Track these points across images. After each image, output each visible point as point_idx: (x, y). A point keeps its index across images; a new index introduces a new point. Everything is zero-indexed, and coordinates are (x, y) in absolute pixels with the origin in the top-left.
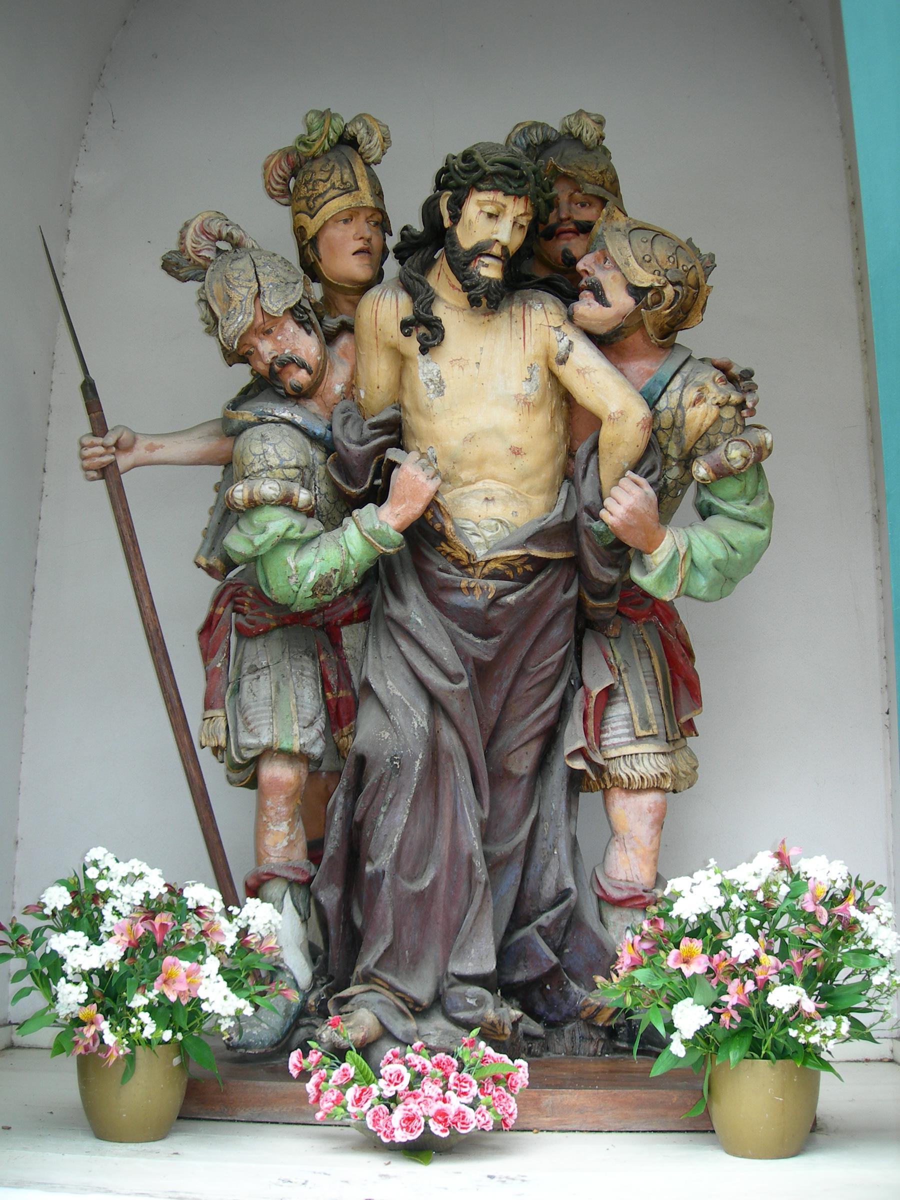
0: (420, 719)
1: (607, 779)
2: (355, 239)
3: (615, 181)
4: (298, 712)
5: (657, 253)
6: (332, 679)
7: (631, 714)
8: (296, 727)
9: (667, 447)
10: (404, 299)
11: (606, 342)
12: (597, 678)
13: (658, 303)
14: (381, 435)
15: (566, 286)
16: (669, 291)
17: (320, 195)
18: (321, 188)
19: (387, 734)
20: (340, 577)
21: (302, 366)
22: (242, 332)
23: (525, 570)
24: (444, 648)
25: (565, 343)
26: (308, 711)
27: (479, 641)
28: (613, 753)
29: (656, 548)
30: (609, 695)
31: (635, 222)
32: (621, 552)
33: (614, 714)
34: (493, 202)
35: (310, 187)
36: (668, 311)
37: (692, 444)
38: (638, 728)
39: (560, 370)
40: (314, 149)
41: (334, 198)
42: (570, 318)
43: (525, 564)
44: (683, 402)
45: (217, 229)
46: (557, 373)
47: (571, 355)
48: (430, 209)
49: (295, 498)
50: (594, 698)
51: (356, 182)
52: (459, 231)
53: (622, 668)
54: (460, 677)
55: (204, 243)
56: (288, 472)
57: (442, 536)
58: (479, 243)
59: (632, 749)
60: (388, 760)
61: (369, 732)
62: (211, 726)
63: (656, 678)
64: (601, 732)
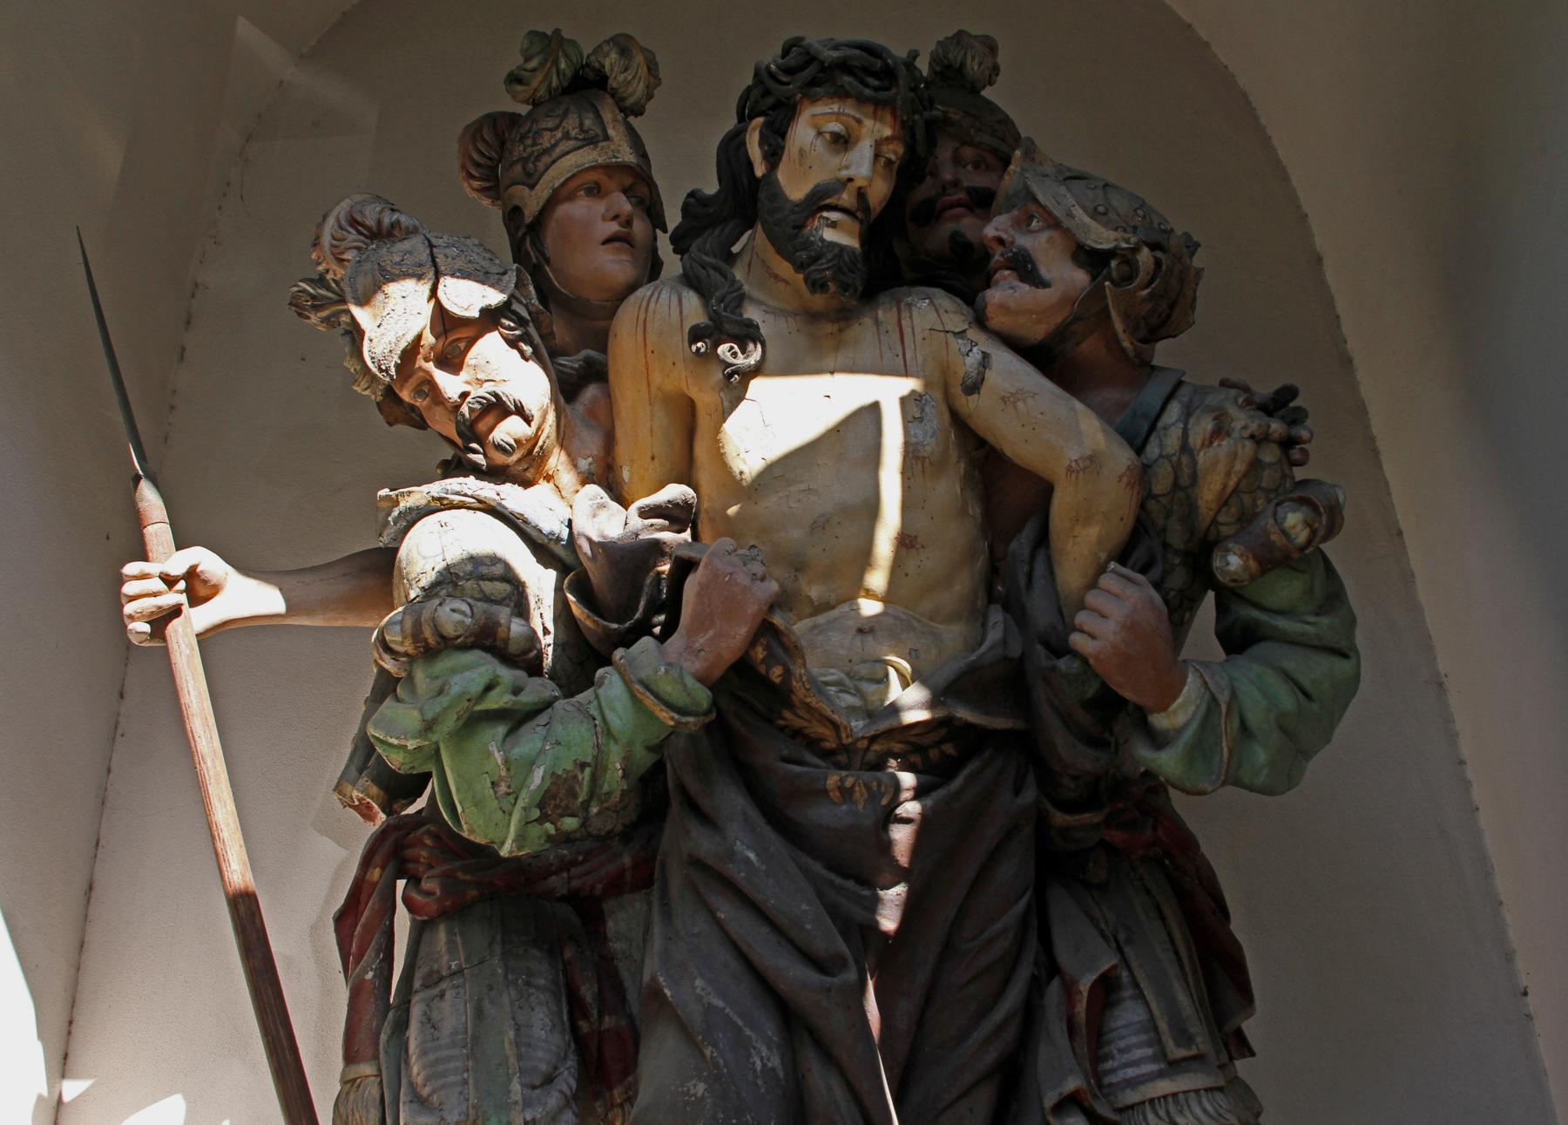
0: (765, 1052)
2: (604, 219)
4: (520, 1057)
5: (1115, 203)
6: (588, 992)
7: (1152, 1018)
8: (516, 1086)
9: (1164, 530)
10: (692, 300)
11: (1044, 356)
12: (1085, 957)
13: (1129, 278)
15: (965, 274)
16: (1145, 257)
17: (546, 151)
18: (546, 140)
20: (594, 779)
22: (403, 345)
23: (942, 753)
24: (804, 907)
25: (976, 355)
26: (540, 1054)
28: (1131, 1097)
29: (1175, 698)
30: (1107, 988)
31: (1069, 169)
32: (1112, 712)
33: (1120, 1023)
34: (838, 116)
35: (529, 142)
36: (1146, 292)
37: (1211, 513)
38: (1170, 1044)
39: (970, 405)
40: (535, 84)
41: (568, 153)
42: (980, 321)
44: (1191, 440)
45: (375, 216)
47: (988, 374)
48: (731, 152)
49: (501, 632)
50: (1085, 994)
51: (604, 130)
52: (781, 175)
53: (1121, 937)
54: (841, 963)
55: (351, 237)
56: (487, 586)
57: (780, 695)
58: (818, 185)
59: (1164, 1087)
62: (352, 1097)
63: (1177, 953)
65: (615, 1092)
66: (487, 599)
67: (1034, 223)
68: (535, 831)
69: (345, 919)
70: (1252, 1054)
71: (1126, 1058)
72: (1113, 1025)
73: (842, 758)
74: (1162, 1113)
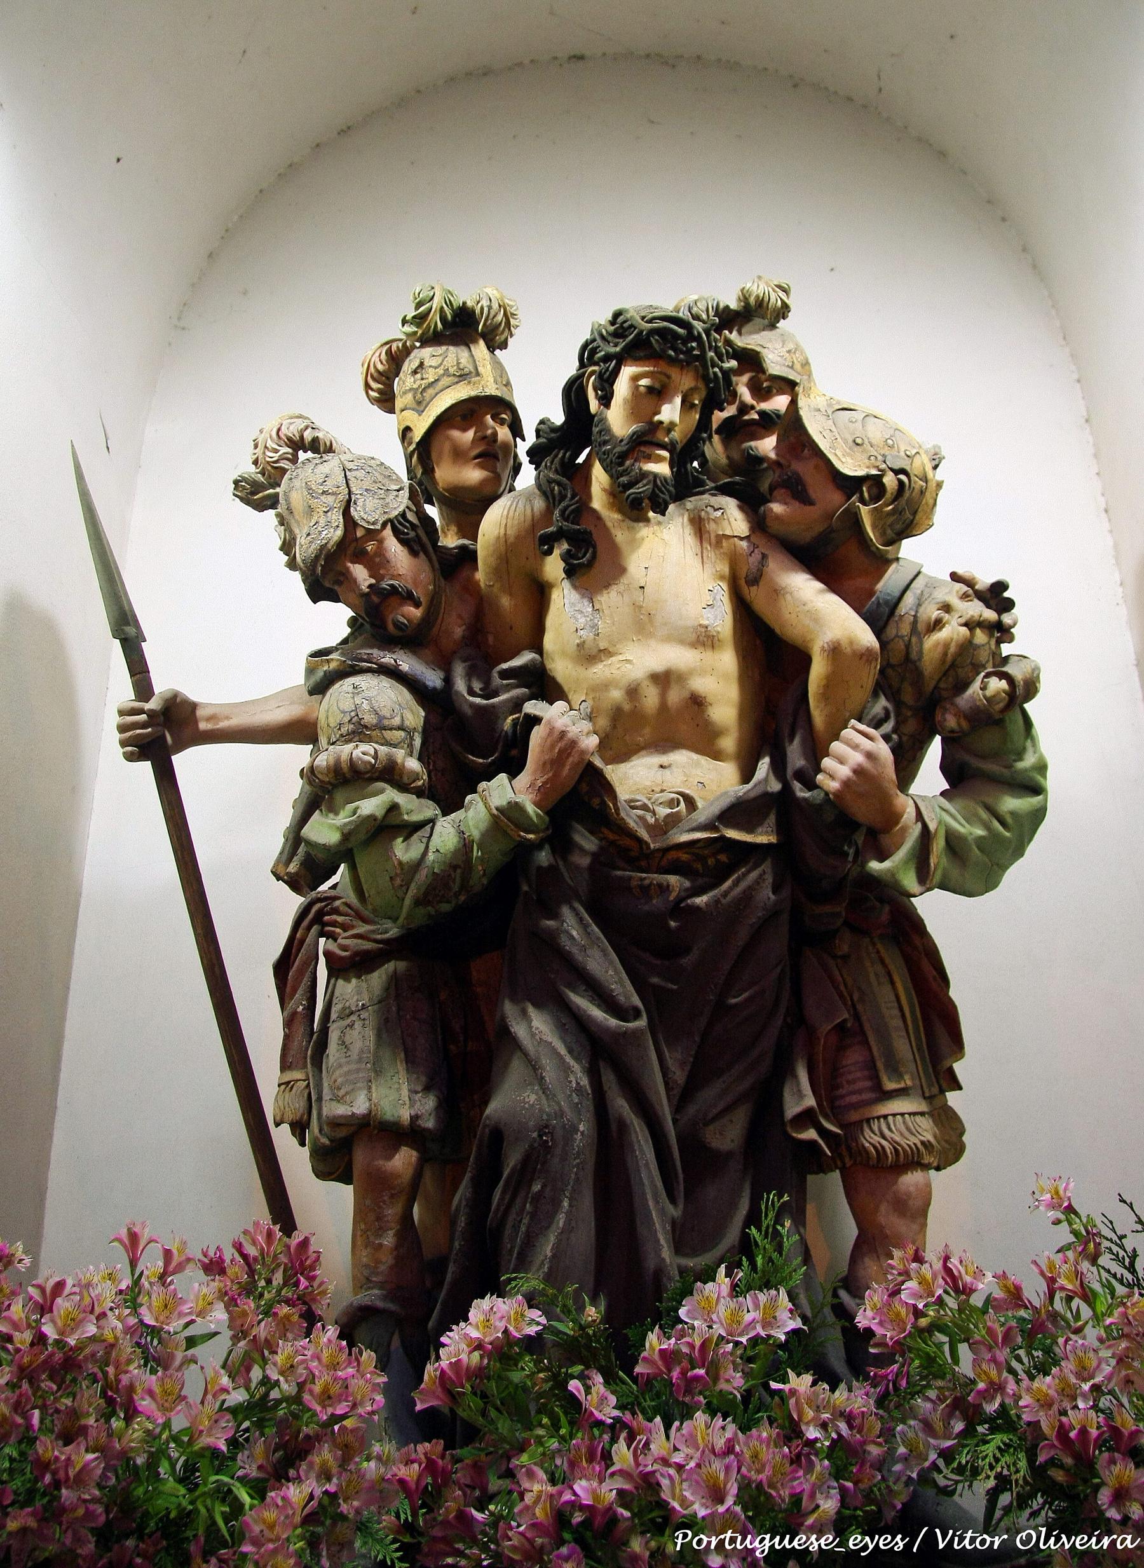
0: (579, 1075)
1: (845, 1153)
3: (806, 364)
14: (518, 686)
19: (533, 1098)
21: (409, 598)
23: (718, 861)
27: (659, 962)
31: (838, 403)
43: (719, 851)
46: (748, 598)
48: (573, 393)
54: (637, 1015)
60: (535, 1135)
61: (513, 1099)
64: (837, 1087)
65: (475, 1097)
66: (387, 743)
67: (806, 451)
68: (421, 911)
69: (282, 968)
70: (960, 1088)
71: (852, 1087)
72: (844, 1063)
73: (643, 864)
74: (875, 1128)
